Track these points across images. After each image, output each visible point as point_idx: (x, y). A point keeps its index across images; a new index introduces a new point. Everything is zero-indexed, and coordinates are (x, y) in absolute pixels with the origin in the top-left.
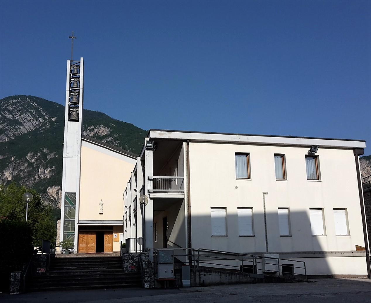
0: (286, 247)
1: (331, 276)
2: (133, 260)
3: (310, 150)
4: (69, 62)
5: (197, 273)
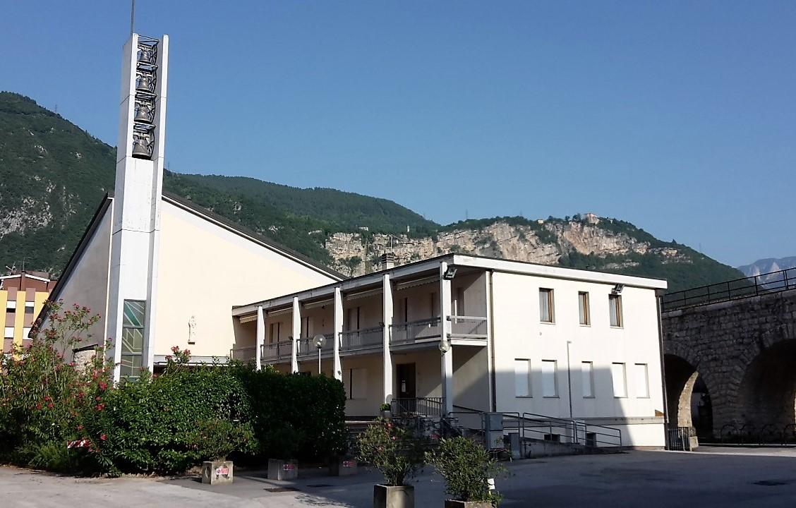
0: (590, 410)
1: (631, 448)
2: (434, 427)
3: (615, 289)
4: (135, 38)
5: (523, 443)
